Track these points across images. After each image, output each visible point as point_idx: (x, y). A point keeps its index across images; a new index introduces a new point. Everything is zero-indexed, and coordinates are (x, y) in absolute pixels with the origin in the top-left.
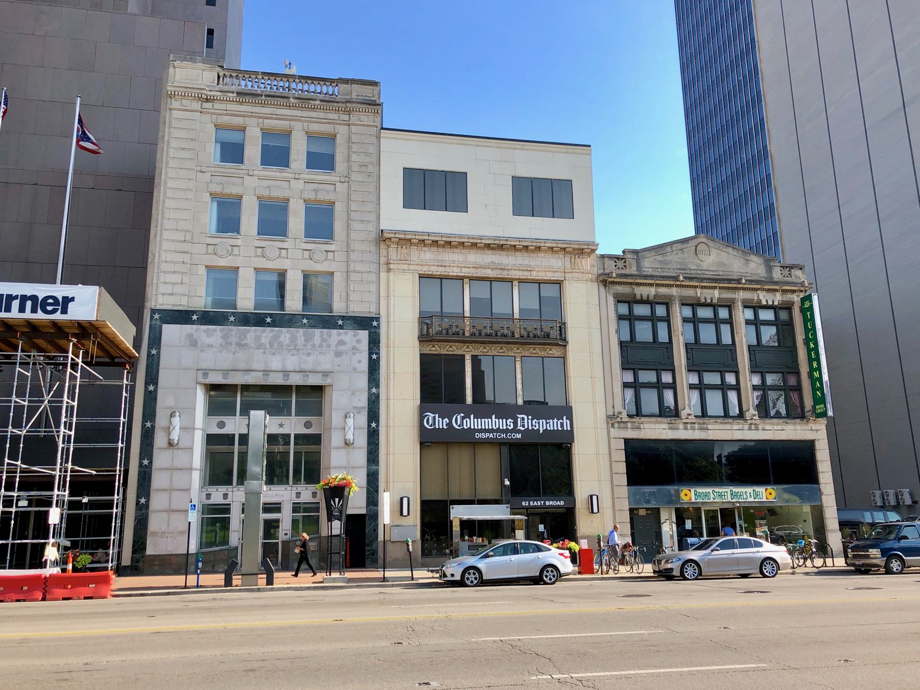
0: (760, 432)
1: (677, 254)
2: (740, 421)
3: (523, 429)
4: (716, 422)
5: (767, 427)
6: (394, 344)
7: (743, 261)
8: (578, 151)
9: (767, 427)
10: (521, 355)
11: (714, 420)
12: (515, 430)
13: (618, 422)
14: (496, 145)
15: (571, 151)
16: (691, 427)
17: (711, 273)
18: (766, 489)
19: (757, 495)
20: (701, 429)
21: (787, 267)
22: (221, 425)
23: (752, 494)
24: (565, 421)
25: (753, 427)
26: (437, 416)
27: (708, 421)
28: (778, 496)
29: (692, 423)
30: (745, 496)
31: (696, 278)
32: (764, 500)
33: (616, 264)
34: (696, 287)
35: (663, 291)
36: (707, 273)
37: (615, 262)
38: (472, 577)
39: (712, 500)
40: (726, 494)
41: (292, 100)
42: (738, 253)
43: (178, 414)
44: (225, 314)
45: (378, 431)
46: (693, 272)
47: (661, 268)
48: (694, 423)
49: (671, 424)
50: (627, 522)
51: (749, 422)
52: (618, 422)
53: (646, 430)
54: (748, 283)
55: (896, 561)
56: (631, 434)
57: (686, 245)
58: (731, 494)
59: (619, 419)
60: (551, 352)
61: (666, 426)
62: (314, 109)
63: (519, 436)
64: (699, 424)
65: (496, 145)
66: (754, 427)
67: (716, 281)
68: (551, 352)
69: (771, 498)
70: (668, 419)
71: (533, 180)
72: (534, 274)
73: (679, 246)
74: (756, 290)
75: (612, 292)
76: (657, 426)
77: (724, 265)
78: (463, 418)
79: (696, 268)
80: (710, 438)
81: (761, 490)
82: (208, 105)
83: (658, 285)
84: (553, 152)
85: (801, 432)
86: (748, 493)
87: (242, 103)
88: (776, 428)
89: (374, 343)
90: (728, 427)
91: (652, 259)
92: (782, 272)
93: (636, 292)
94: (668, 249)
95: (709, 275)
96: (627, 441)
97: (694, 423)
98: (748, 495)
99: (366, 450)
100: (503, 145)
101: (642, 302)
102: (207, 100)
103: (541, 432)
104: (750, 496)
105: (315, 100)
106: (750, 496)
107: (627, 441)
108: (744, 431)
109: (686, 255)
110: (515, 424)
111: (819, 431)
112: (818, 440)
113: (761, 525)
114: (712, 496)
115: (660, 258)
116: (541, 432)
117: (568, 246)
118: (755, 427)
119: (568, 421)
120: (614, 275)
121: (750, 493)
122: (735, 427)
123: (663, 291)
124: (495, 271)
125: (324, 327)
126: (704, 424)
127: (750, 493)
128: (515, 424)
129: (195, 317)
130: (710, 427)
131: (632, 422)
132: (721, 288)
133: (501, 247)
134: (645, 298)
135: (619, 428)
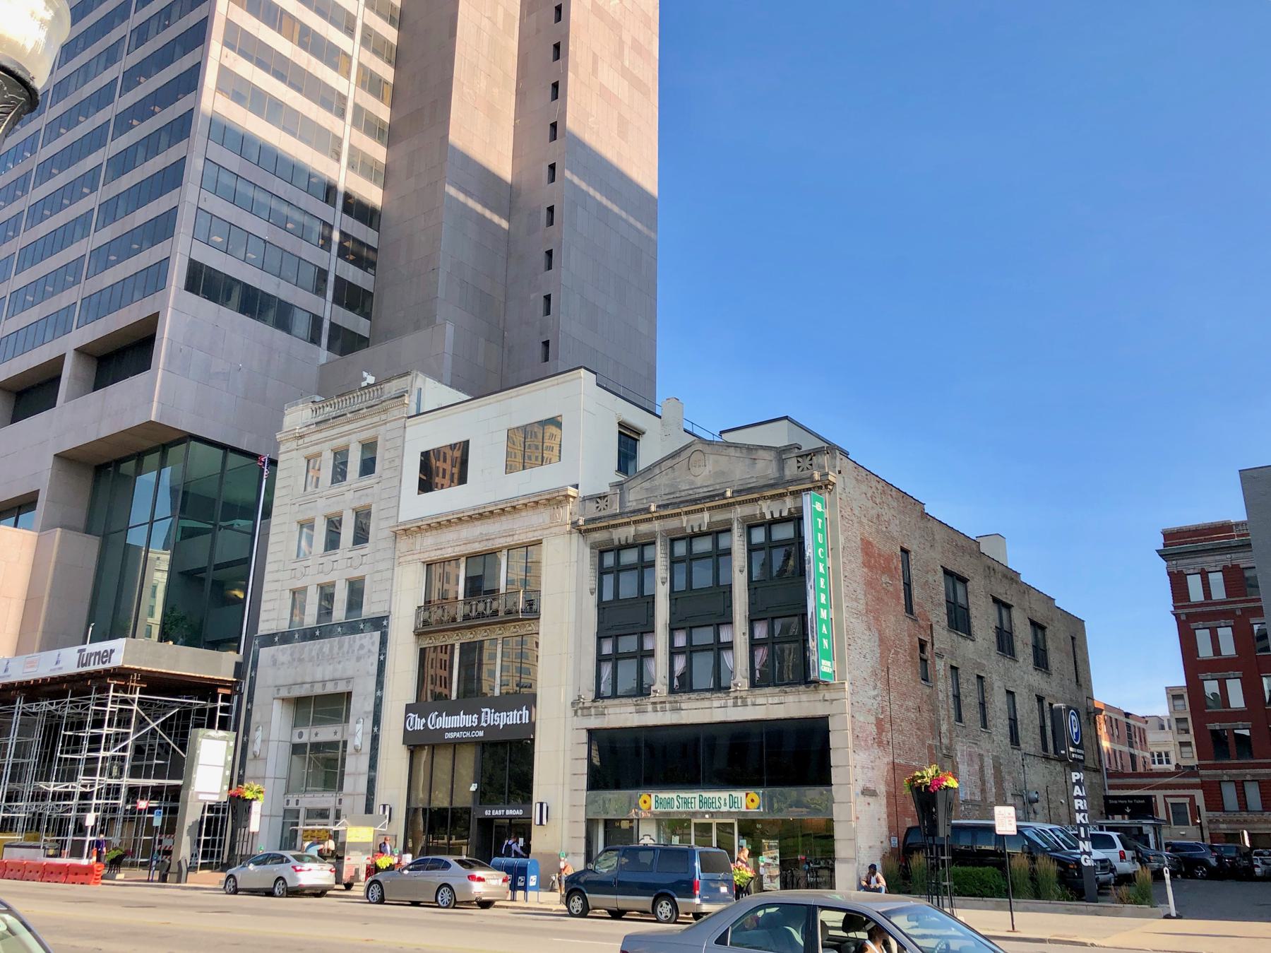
0: (750, 708)
1: (667, 474)
2: (720, 695)
3: (485, 725)
4: (689, 699)
5: (759, 701)
6: (396, 642)
7: (748, 461)
8: (568, 378)
9: (759, 701)
10: (502, 636)
11: (688, 696)
12: (479, 728)
13: (582, 709)
14: (494, 400)
15: (562, 380)
16: (661, 707)
17: (705, 490)
18: (747, 794)
19: (733, 802)
20: (673, 710)
21: (807, 455)
22: (301, 735)
23: (727, 801)
24: (525, 712)
25: (739, 701)
26: (417, 715)
27: (680, 698)
28: (769, 803)
29: (661, 703)
30: (718, 804)
31: (671, 504)
32: (744, 809)
33: (597, 505)
34: (679, 514)
35: (644, 528)
36: (701, 490)
37: (598, 503)
38: (445, 896)
39: (675, 809)
40: (693, 800)
41: (349, 415)
42: (741, 452)
43: (261, 728)
44: (353, 624)
45: (378, 735)
46: (683, 494)
47: (647, 498)
48: (664, 702)
49: (638, 705)
50: (580, 838)
51: (732, 695)
52: (582, 709)
53: (610, 716)
54: (735, 495)
55: (667, 904)
56: (595, 723)
57: (677, 460)
58: (700, 801)
59: (581, 705)
60: (530, 628)
61: (632, 709)
62: (364, 418)
63: (481, 734)
64: (670, 702)
65: (494, 400)
66: (741, 702)
67: (696, 502)
68: (530, 628)
69: (753, 808)
70: (634, 699)
71: (123, 533)
72: (516, 537)
73: (669, 463)
74: (756, 500)
75: (589, 542)
76: (623, 709)
77: (723, 473)
78: (437, 717)
79: (688, 487)
80: (683, 722)
81: (740, 794)
82: (301, 442)
83: (635, 522)
84: (545, 388)
85: (807, 704)
86: (723, 799)
87: (320, 431)
88: (770, 700)
89: (383, 642)
90: (706, 704)
91: (638, 488)
92: (799, 465)
93: (614, 537)
94: (657, 471)
95: (702, 492)
96: (591, 732)
97: (664, 702)
98: (722, 802)
99: (369, 756)
100: (568, 378)
101: (628, 546)
102: (301, 437)
103: (501, 727)
104: (725, 803)
105: (362, 409)
106: (725, 803)
107: (591, 732)
108: (728, 709)
109: (677, 473)
110: (479, 719)
111: (834, 702)
112: (834, 715)
113: (770, 847)
114: (676, 803)
115: (647, 485)
116: (501, 727)
117: (540, 498)
118: (742, 702)
119: (527, 712)
120: (729, 494)
121: (725, 800)
122: (716, 704)
123: (644, 528)
124: (482, 543)
125: (352, 634)
126: (676, 702)
127: (725, 800)
128: (479, 719)
129: (276, 639)
130: (684, 706)
131: (595, 707)
132: (709, 509)
133: (481, 516)
134: (630, 541)
135: (583, 715)
